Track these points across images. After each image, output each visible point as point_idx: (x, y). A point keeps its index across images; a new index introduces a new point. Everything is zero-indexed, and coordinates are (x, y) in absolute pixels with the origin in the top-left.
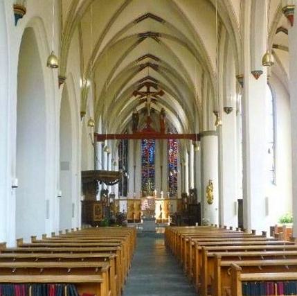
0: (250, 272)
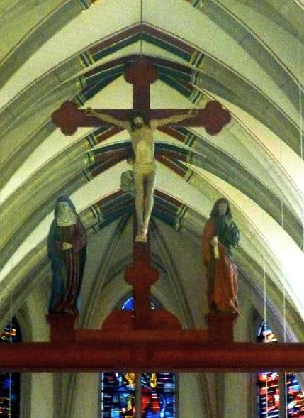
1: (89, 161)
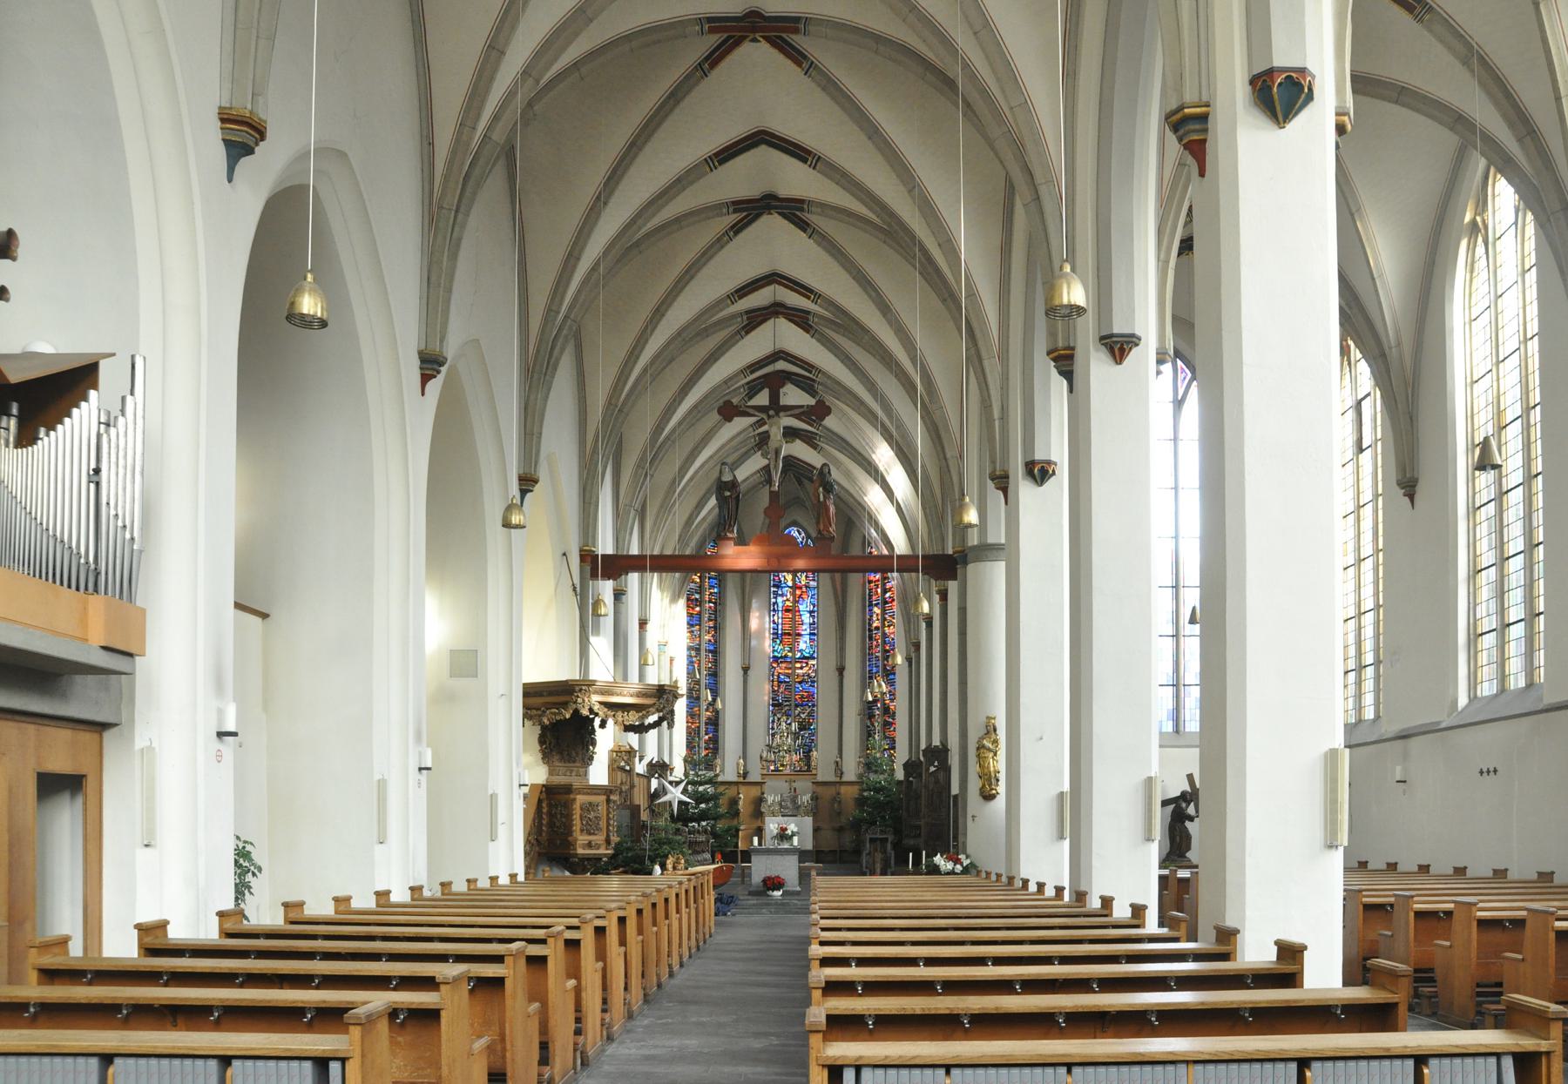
0: (1118, 1035)
1: (755, 441)
